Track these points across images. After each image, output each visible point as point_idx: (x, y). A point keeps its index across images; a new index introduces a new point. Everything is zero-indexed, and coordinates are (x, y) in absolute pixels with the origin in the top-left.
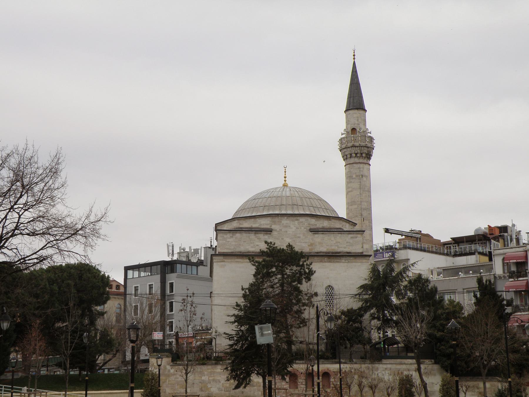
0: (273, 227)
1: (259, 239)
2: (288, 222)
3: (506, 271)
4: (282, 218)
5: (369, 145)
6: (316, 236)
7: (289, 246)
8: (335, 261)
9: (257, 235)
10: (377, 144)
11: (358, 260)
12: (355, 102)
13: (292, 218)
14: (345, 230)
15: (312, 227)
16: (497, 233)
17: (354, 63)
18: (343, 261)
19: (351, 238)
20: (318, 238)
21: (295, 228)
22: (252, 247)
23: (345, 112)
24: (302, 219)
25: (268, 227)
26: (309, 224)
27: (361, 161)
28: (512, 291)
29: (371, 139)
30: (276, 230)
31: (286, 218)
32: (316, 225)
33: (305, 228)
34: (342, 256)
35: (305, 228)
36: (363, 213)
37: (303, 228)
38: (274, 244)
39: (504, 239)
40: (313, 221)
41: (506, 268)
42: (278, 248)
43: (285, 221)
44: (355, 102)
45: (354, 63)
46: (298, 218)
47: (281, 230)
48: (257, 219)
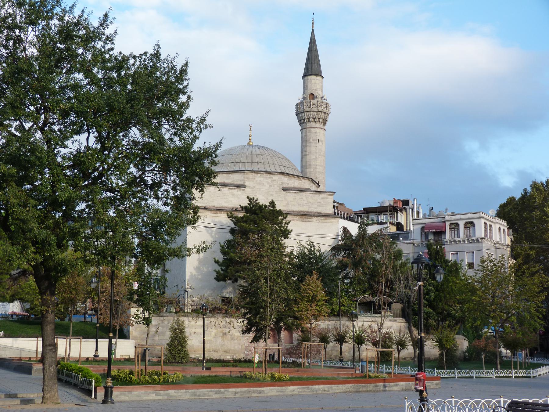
0: (247, 183)
1: (233, 194)
2: (261, 179)
3: (424, 239)
4: (256, 175)
5: (325, 110)
6: (288, 194)
7: (272, 203)
8: (307, 220)
9: (231, 190)
10: (332, 110)
11: (315, 219)
12: (312, 67)
13: (265, 176)
14: (312, 190)
15: (285, 186)
16: (400, 205)
17: (313, 31)
18: (315, 220)
19: (323, 198)
20: (291, 196)
21: (268, 186)
22: (226, 202)
23: (303, 78)
24: (276, 177)
25: (241, 183)
26: (282, 183)
27: (318, 125)
28: (473, 259)
29: (327, 106)
30: (249, 187)
31: (259, 175)
32: (288, 184)
33: (278, 187)
34: (314, 216)
35: (278, 187)
36: (318, 176)
37: (276, 186)
38: (257, 200)
39: (406, 212)
40: (285, 179)
41: (424, 236)
42: (261, 204)
43: (259, 178)
44: (312, 67)
45: (313, 31)
46: (272, 176)
47: (255, 187)
48: (230, 175)
